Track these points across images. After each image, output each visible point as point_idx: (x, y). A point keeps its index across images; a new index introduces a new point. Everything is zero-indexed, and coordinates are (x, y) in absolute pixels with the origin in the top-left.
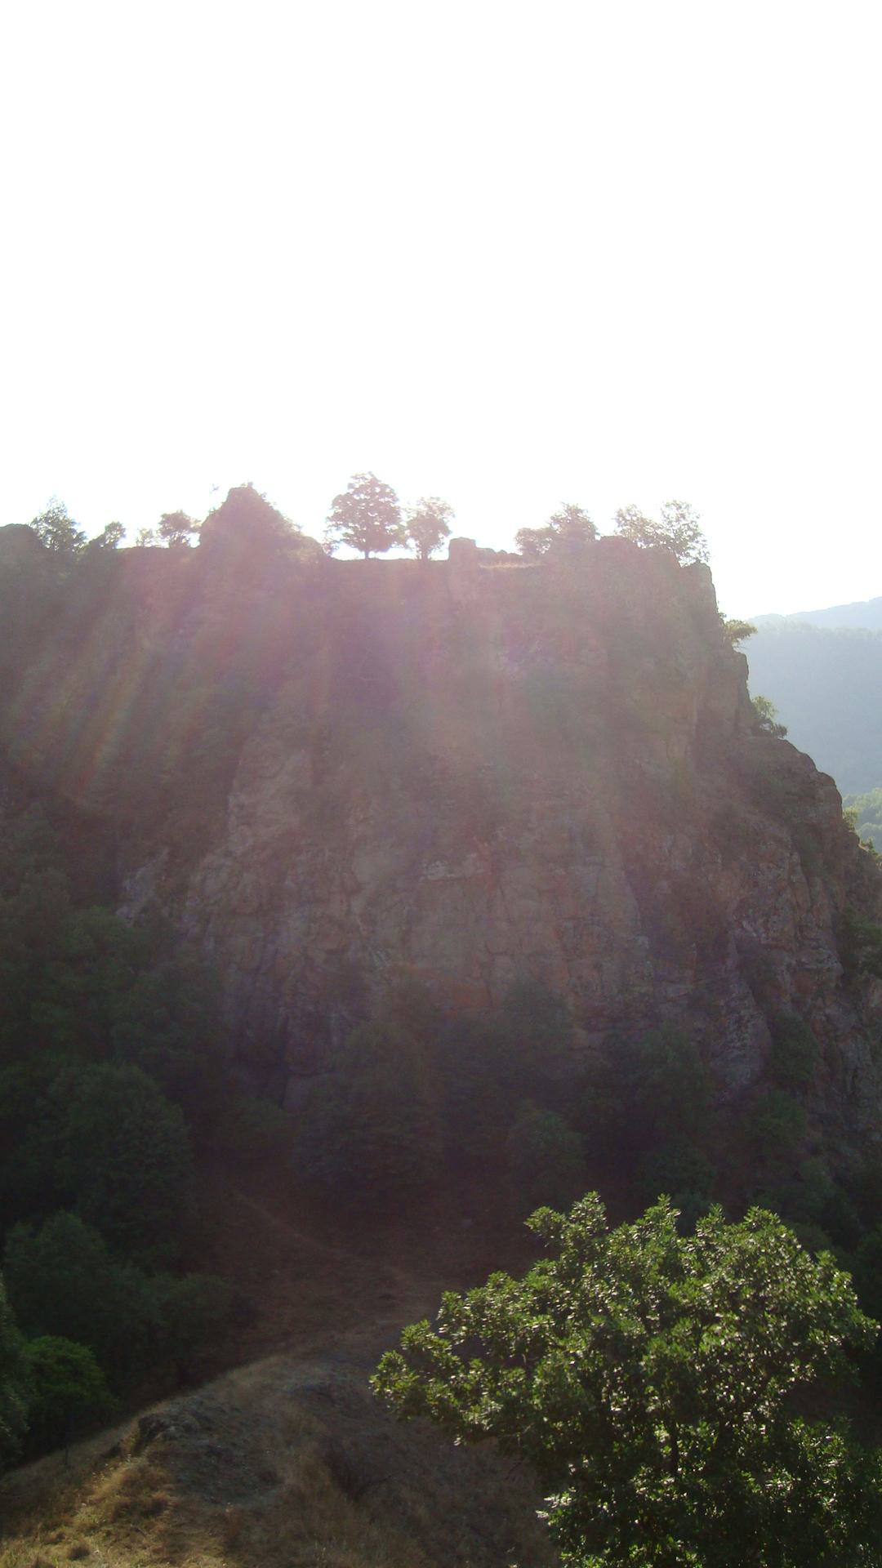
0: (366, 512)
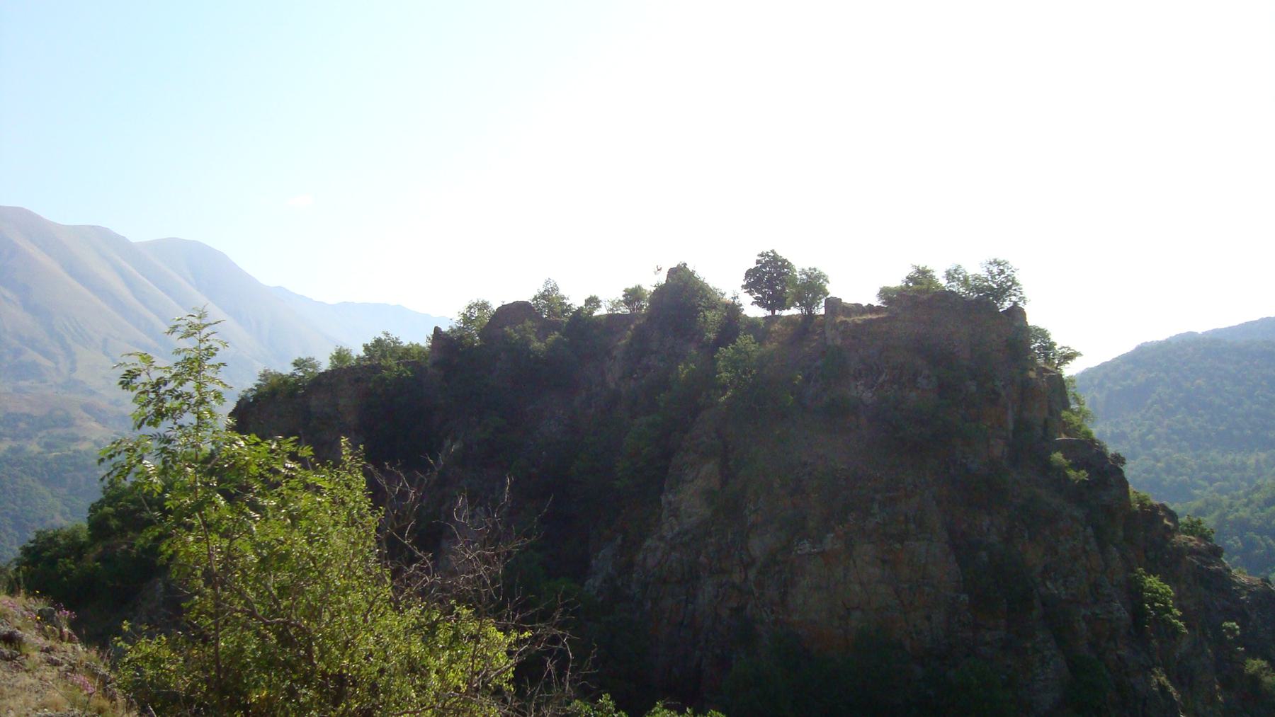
0: (770, 277)
